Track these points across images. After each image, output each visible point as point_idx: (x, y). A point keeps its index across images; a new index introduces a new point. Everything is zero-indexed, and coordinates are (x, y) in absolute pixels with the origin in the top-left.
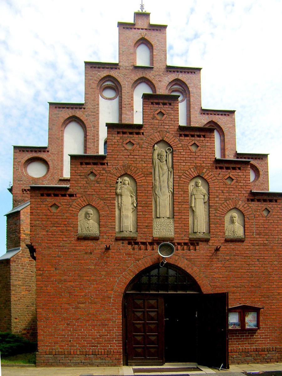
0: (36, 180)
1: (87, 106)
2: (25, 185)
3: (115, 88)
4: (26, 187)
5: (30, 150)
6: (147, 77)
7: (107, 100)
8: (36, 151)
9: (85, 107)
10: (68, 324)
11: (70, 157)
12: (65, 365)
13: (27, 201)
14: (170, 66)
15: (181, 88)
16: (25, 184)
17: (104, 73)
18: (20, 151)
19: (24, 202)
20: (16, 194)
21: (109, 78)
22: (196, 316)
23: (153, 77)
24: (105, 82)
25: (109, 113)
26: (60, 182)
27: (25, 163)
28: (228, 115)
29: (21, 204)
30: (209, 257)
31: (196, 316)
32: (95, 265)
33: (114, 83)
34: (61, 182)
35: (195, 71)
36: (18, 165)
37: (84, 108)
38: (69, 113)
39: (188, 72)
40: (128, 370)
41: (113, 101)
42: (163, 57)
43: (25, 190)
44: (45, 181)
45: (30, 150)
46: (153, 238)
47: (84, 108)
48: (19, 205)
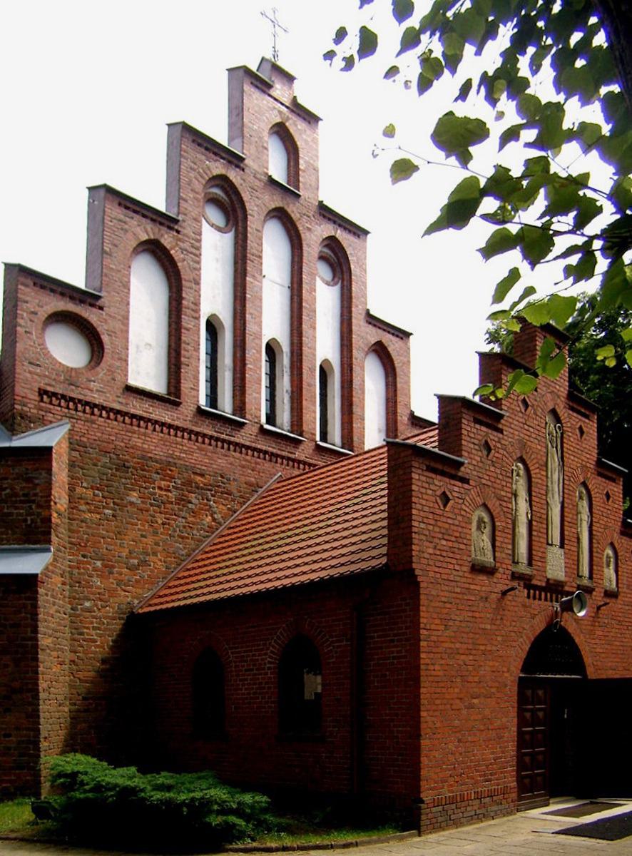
0: (73, 374)
1: (184, 228)
2: (47, 381)
3: (229, 209)
4: (49, 385)
5: (60, 290)
6: (289, 210)
7: (213, 229)
8: (72, 298)
9: (180, 229)
10: (460, 741)
11: (437, 400)
12: (457, 824)
13: (51, 422)
14: (326, 206)
15: (332, 255)
16: (45, 376)
17: (218, 168)
18: (35, 284)
19: (46, 425)
20: (23, 397)
21: (222, 182)
22: (565, 716)
23: (298, 215)
24: (212, 186)
25: (217, 260)
26: (126, 393)
27: (47, 319)
28: (402, 338)
29: (35, 428)
30: (592, 619)
31: (565, 716)
32: (491, 624)
33: (228, 196)
34: (129, 393)
35: (360, 233)
36: (31, 320)
37: (178, 232)
38: (144, 231)
39: (350, 231)
40: (545, 821)
41: (224, 235)
42: (313, 178)
43: (46, 392)
44: (94, 382)
45: (60, 290)
46: (548, 580)
47: (178, 232)
48: (31, 428)
